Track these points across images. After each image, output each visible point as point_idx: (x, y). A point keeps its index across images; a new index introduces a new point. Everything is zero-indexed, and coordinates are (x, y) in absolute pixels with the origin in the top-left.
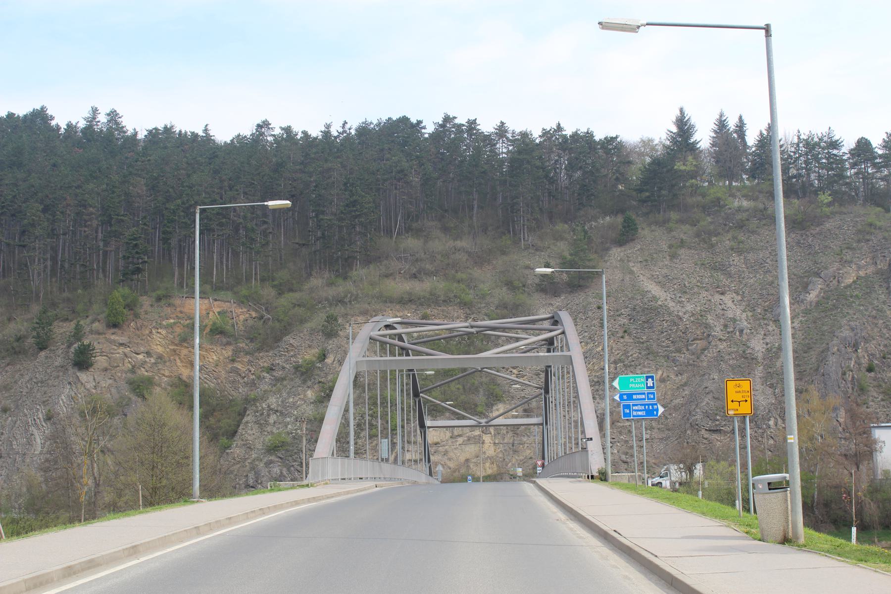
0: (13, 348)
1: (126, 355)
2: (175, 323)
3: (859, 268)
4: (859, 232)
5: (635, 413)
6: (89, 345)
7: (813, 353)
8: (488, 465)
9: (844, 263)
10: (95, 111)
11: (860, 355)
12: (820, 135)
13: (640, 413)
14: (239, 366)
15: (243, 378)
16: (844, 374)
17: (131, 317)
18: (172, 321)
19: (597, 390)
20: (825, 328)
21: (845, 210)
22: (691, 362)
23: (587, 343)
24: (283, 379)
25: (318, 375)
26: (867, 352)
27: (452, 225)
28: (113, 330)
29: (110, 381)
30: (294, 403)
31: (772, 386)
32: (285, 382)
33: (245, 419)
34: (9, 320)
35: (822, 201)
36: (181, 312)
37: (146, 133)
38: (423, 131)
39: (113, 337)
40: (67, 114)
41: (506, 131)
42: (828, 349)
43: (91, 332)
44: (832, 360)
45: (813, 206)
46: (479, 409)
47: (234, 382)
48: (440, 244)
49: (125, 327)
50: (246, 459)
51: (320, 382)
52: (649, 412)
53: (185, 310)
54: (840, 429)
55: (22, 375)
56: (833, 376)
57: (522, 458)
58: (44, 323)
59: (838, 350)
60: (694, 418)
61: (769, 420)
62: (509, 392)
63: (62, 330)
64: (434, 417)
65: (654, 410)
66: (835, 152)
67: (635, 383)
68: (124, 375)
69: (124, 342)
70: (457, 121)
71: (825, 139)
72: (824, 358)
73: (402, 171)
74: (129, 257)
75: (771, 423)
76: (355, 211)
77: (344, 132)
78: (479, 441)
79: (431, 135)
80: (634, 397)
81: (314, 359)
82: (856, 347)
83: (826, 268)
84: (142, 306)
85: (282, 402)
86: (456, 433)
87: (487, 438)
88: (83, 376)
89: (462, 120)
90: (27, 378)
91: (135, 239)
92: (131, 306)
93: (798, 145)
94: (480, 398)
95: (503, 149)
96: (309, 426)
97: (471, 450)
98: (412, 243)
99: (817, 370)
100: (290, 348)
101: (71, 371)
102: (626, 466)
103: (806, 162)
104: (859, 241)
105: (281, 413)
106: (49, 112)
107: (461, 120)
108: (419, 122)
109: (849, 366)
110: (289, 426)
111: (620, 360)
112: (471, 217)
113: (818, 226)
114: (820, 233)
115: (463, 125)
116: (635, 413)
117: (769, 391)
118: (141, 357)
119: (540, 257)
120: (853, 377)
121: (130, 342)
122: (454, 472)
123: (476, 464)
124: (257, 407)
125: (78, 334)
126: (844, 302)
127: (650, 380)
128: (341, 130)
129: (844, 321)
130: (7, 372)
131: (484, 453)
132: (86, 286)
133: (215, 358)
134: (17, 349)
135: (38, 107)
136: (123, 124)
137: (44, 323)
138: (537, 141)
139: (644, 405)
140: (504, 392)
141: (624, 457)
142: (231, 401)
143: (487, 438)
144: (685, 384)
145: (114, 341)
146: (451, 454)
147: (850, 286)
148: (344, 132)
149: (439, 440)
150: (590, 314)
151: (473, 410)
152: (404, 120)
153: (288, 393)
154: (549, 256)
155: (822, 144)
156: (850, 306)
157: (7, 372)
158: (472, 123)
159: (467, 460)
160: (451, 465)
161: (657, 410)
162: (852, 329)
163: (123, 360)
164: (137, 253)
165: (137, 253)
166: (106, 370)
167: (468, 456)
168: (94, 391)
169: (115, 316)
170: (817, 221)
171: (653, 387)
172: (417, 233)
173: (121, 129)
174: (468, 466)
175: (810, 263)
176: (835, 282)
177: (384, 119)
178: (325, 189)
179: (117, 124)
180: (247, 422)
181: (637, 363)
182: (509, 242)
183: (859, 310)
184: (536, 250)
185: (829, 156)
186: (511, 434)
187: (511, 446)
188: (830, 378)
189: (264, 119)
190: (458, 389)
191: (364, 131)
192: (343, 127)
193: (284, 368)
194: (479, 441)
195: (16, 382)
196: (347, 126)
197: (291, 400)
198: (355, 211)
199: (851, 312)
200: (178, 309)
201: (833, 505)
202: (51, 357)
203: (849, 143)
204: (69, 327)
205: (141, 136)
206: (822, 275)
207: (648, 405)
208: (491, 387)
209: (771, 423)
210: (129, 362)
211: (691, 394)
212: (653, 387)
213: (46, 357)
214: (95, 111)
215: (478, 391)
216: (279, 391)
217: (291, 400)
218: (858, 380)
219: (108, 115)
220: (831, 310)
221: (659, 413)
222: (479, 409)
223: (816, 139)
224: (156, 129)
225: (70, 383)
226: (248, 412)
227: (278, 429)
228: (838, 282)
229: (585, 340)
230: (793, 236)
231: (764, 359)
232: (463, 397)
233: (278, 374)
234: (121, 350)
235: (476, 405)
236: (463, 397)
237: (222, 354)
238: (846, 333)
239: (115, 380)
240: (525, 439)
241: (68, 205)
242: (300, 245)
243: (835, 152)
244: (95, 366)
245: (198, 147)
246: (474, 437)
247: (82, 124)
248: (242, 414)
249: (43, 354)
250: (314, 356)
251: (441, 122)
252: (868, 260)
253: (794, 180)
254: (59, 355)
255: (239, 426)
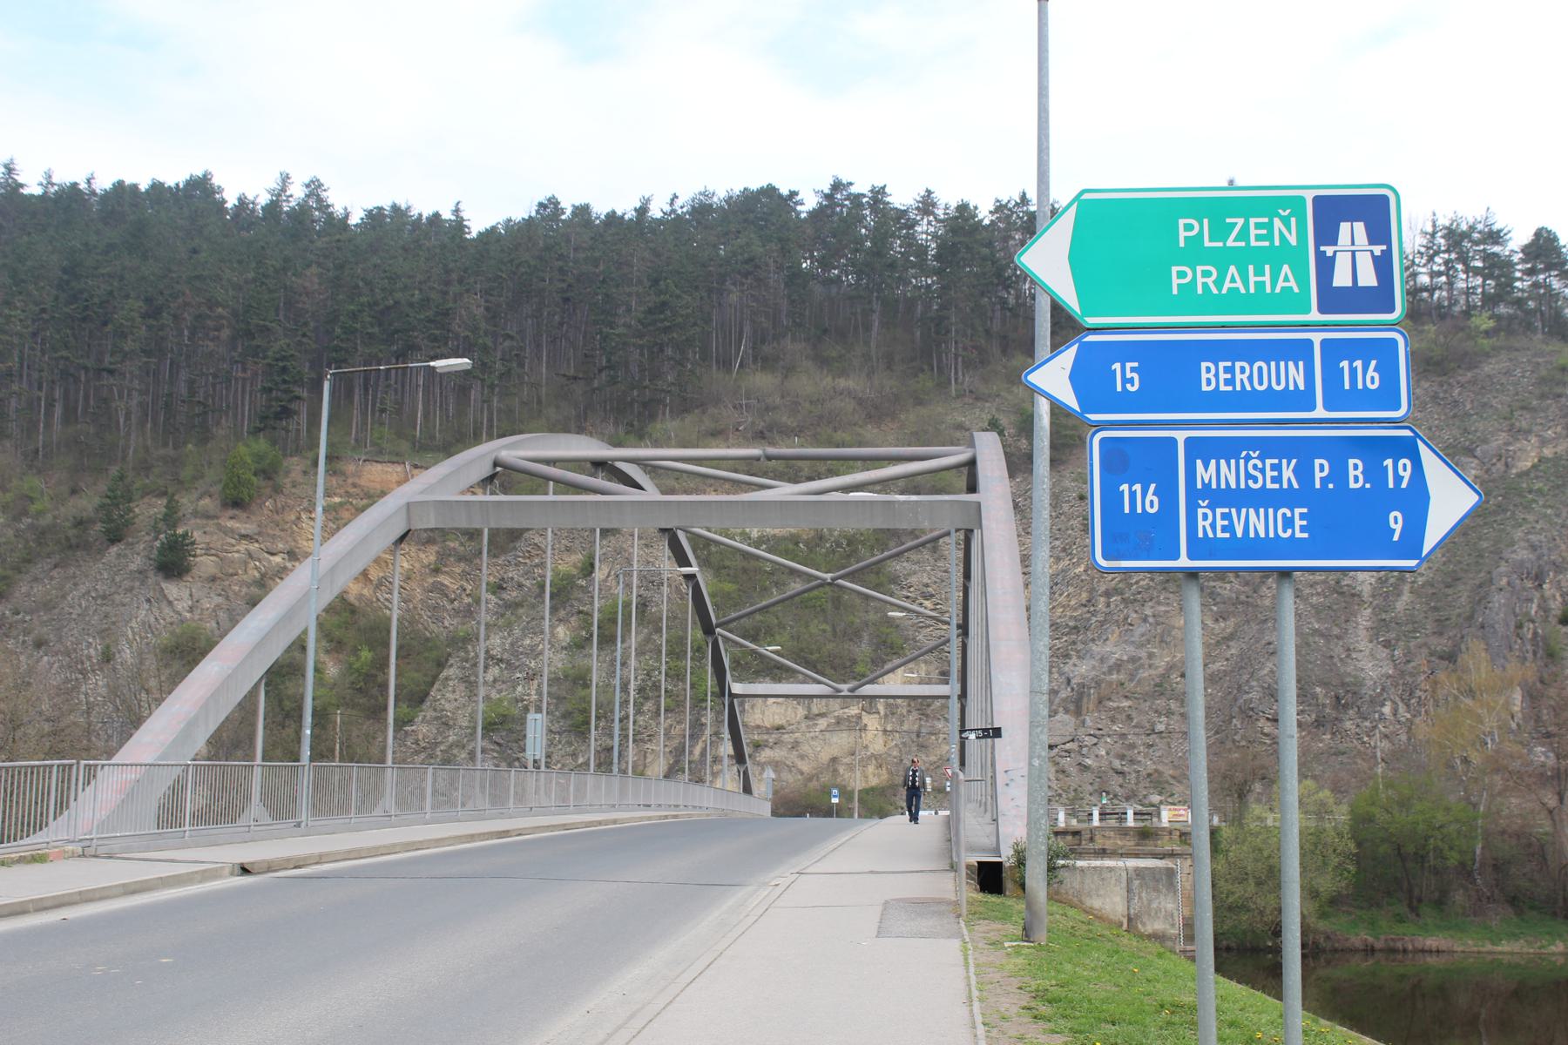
0: (68, 539)
1: (250, 556)
2: (341, 504)
3: (1544, 442)
4: (1542, 381)
5: (1210, 522)
6: (185, 535)
7: (1461, 587)
8: (871, 769)
9: (1517, 433)
10: (285, 179)
11: (1548, 594)
12: (1471, 221)
13: (1257, 523)
14: (446, 580)
15: (452, 601)
16: (1519, 626)
17: (268, 491)
18: (337, 500)
19: (1074, 643)
20: (1485, 544)
21: (1517, 345)
22: (1243, 597)
23: (1058, 559)
24: (518, 605)
25: (579, 600)
26: (1559, 588)
27: (834, 354)
28: (231, 512)
29: (220, 600)
30: (533, 648)
31: (1387, 644)
32: (521, 611)
33: (444, 674)
34: (74, 492)
35: (1477, 327)
36: (354, 485)
37: (362, 214)
38: (799, 208)
39: (230, 524)
40: (244, 182)
41: (934, 205)
42: (1491, 580)
43: (195, 514)
44: (1498, 600)
45: (1460, 335)
46: (859, 668)
47: (435, 608)
48: (809, 382)
49: (254, 507)
50: (437, 744)
51: (580, 612)
52: (1344, 520)
53: (363, 482)
54: (1514, 726)
55: (75, 584)
56: (1500, 628)
57: (933, 758)
58: (119, 498)
59: (1508, 583)
60: (1246, 697)
61: (1383, 705)
62: (914, 640)
63: (148, 510)
64: (739, 680)
65: (1380, 497)
66: (1496, 249)
67: (1221, 260)
68: (244, 590)
69: (249, 532)
70: (854, 190)
71: (1480, 227)
72: (1484, 598)
73: (751, 260)
74: (270, 390)
75: (1387, 710)
76: (662, 321)
77: (673, 211)
78: (856, 725)
79: (813, 214)
80: (1211, 376)
81: (575, 572)
82: (1539, 579)
83: (1485, 441)
84: (288, 473)
85: (512, 644)
86: (815, 710)
87: (872, 722)
88: (172, 589)
89: (862, 187)
90: (83, 589)
91: (284, 358)
92: (268, 472)
93: (1433, 235)
94: (863, 649)
95: (924, 230)
96: (554, 689)
97: (841, 741)
98: (762, 381)
99: (1471, 618)
100: (534, 552)
101: (153, 578)
102: (1120, 780)
103: (1446, 262)
104: (1543, 396)
105: (508, 663)
106: (216, 181)
107: (861, 187)
108: (793, 194)
109: (1528, 613)
110: (520, 688)
111: (1117, 591)
112: (867, 343)
113: (1469, 369)
114: (1474, 382)
115: (864, 196)
116: (1210, 522)
117: (1383, 653)
118: (277, 559)
119: (982, 410)
120: (1535, 634)
121: (259, 534)
122: (810, 779)
123: (851, 767)
124: (467, 652)
125: (171, 517)
126: (1517, 500)
127: (1352, 233)
128: (667, 208)
129: (1518, 534)
130: (52, 578)
131: (866, 747)
132: (205, 439)
133: (406, 565)
134: (74, 541)
135: (200, 174)
136: (330, 201)
137: (119, 498)
138: (986, 222)
139: (1302, 451)
140: (906, 640)
141: (1117, 764)
142: (427, 640)
143: (872, 722)
144: (1231, 637)
145: (232, 530)
146: (805, 748)
147: (1526, 474)
148: (673, 211)
149: (783, 722)
150: (1066, 507)
151: (838, 668)
152: (770, 191)
153: (523, 630)
154: (998, 410)
155: (1476, 236)
156: (1527, 508)
157: (52, 578)
158: (878, 194)
159: (834, 760)
160: (805, 767)
161: (1416, 500)
162: (1533, 548)
163: (246, 563)
164: (285, 381)
165: (285, 381)
166: (213, 579)
167: (835, 752)
168: (188, 615)
169: (235, 487)
170: (1469, 360)
171: (1379, 298)
172: (767, 363)
173: (323, 206)
174: (835, 770)
175: (1456, 432)
176: (1500, 466)
177: (737, 190)
178: (617, 286)
179: (320, 200)
180: (447, 679)
181: (1146, 596)
182: (930, 384)
183: (1545, 515)
184: (977, 399)
185: (1487, 257)
186: (915, 715)
187: (914, 736)
188: (1495, 632)
189: (549, 195)
190: (824, 631)
191: (702, 209)
192: (672, 204)
193: (520, 586)
194: (856, 725)
195: (64, 597)
196: (678, 203)
197: (528, 642)
198: (662, 321)
199: (1531, 518)
200: (350, 481)
201: (1513, 870)
202: (125, 556)
203: (1519, 238)
204: (159, 506)
205: (354, 220)
206: (1478, 452)
207: (1339, 451)
208: (884, 629)
209: (1387, 710)
210: (256, 568)
211: (1241, 656)
212: (1379, 298)
213: (119, 555)
214: (285, 179)
215: (861, 637)
216: (509, 625)
217: (528, 642)
218: (1544, 638)
219: (308, 186)
220: (1495, 513)
221: (1437, 527)
222: (859, 668)
223: (1464, 227)
224: (380, 209)
225: (148, 601)
226: (451, 661)
227: (500, 692)
228: (1507, 465)
229: (1056, 552)
230: (1426, 385)
231: (1373, 596)
232: (830, 646)
233: (512, 595)
234: (243, 546)
235: (854, 662)
236: (830, 646)
237: (419, 560)
238: (1522, 554)
239: (227, 598)
240: (940, 725)
241: (186, 304)
242: (569, 378)
243: (1496, 249)
244: (195, 571)
245: (438, 238)
246: (848, 719)
247: (264, 199)
248: (441, 664)
249: (114, 550)
250: (575, 566)
251: (827, 191)
252: (1559, 429)
253: (1425, 295)
254: (137, 554)
255: (433, 684)
